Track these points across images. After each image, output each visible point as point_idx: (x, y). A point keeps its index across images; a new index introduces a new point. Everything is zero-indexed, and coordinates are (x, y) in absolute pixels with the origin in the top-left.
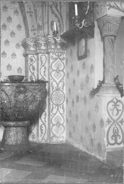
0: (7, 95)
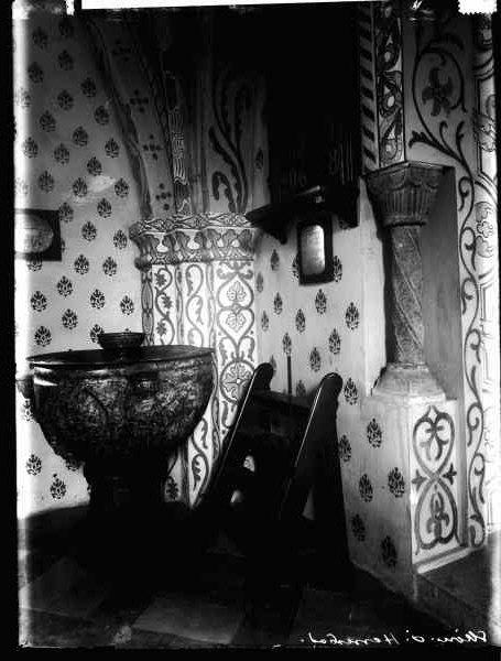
0: (102, 405)
